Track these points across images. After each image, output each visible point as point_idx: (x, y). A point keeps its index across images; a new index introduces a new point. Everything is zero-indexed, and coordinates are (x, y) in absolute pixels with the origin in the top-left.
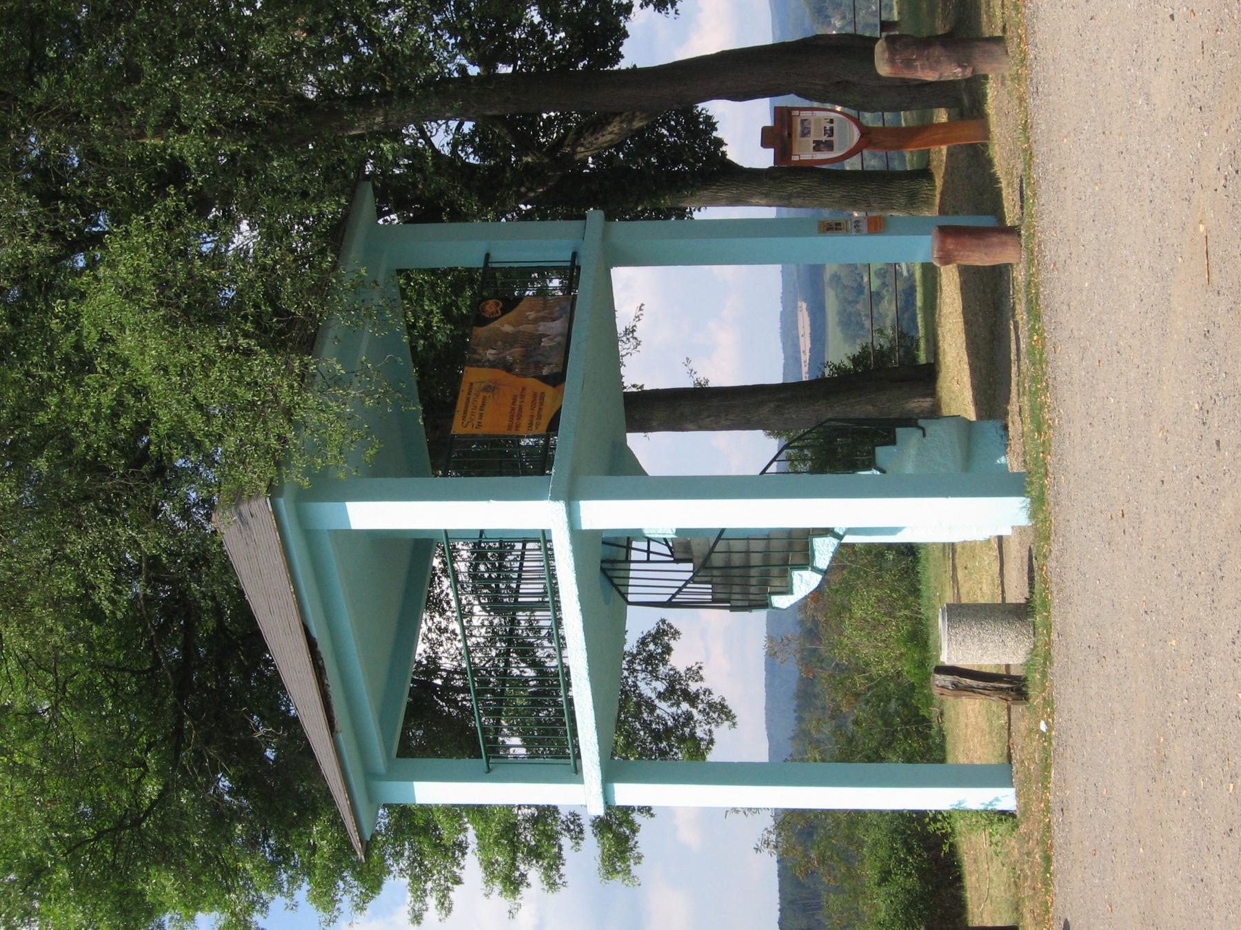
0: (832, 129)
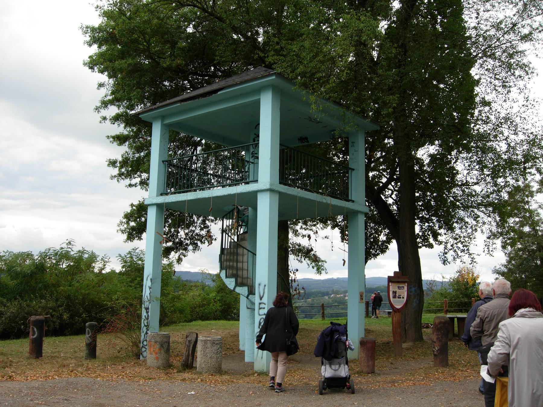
0: (400, 298)
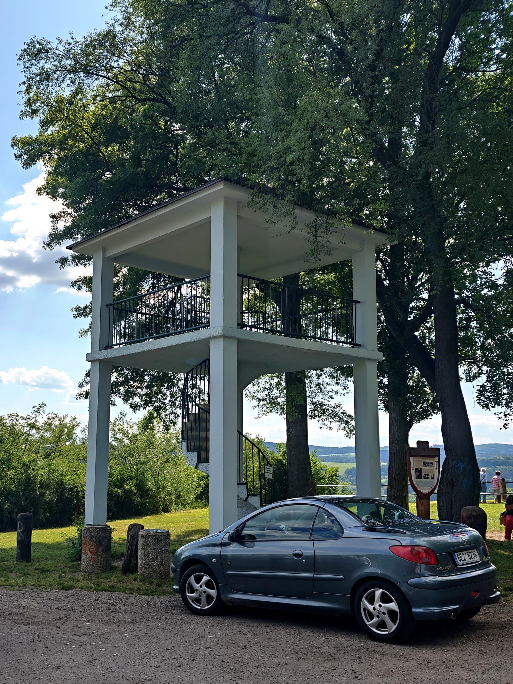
0: (428, 478)
